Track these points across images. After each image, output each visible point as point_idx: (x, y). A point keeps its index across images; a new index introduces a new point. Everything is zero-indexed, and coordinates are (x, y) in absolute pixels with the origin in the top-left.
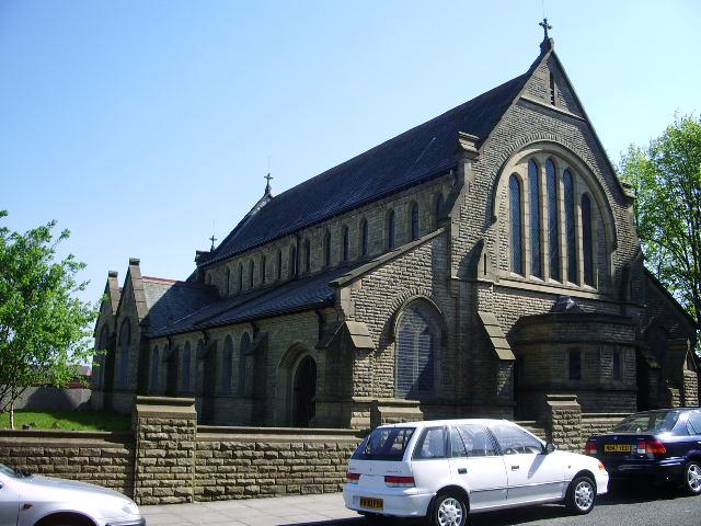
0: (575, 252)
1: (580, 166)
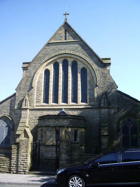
0: (46, 90)
1: (78, 58)
